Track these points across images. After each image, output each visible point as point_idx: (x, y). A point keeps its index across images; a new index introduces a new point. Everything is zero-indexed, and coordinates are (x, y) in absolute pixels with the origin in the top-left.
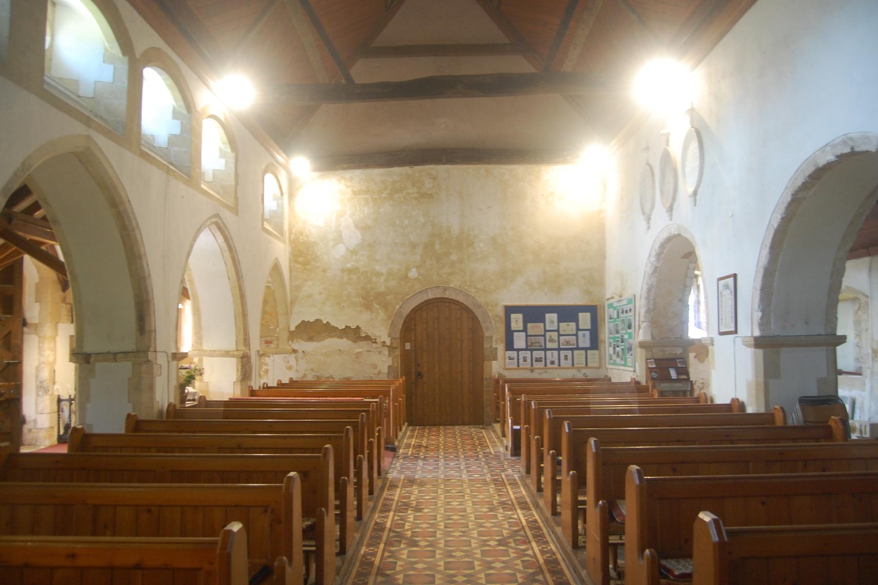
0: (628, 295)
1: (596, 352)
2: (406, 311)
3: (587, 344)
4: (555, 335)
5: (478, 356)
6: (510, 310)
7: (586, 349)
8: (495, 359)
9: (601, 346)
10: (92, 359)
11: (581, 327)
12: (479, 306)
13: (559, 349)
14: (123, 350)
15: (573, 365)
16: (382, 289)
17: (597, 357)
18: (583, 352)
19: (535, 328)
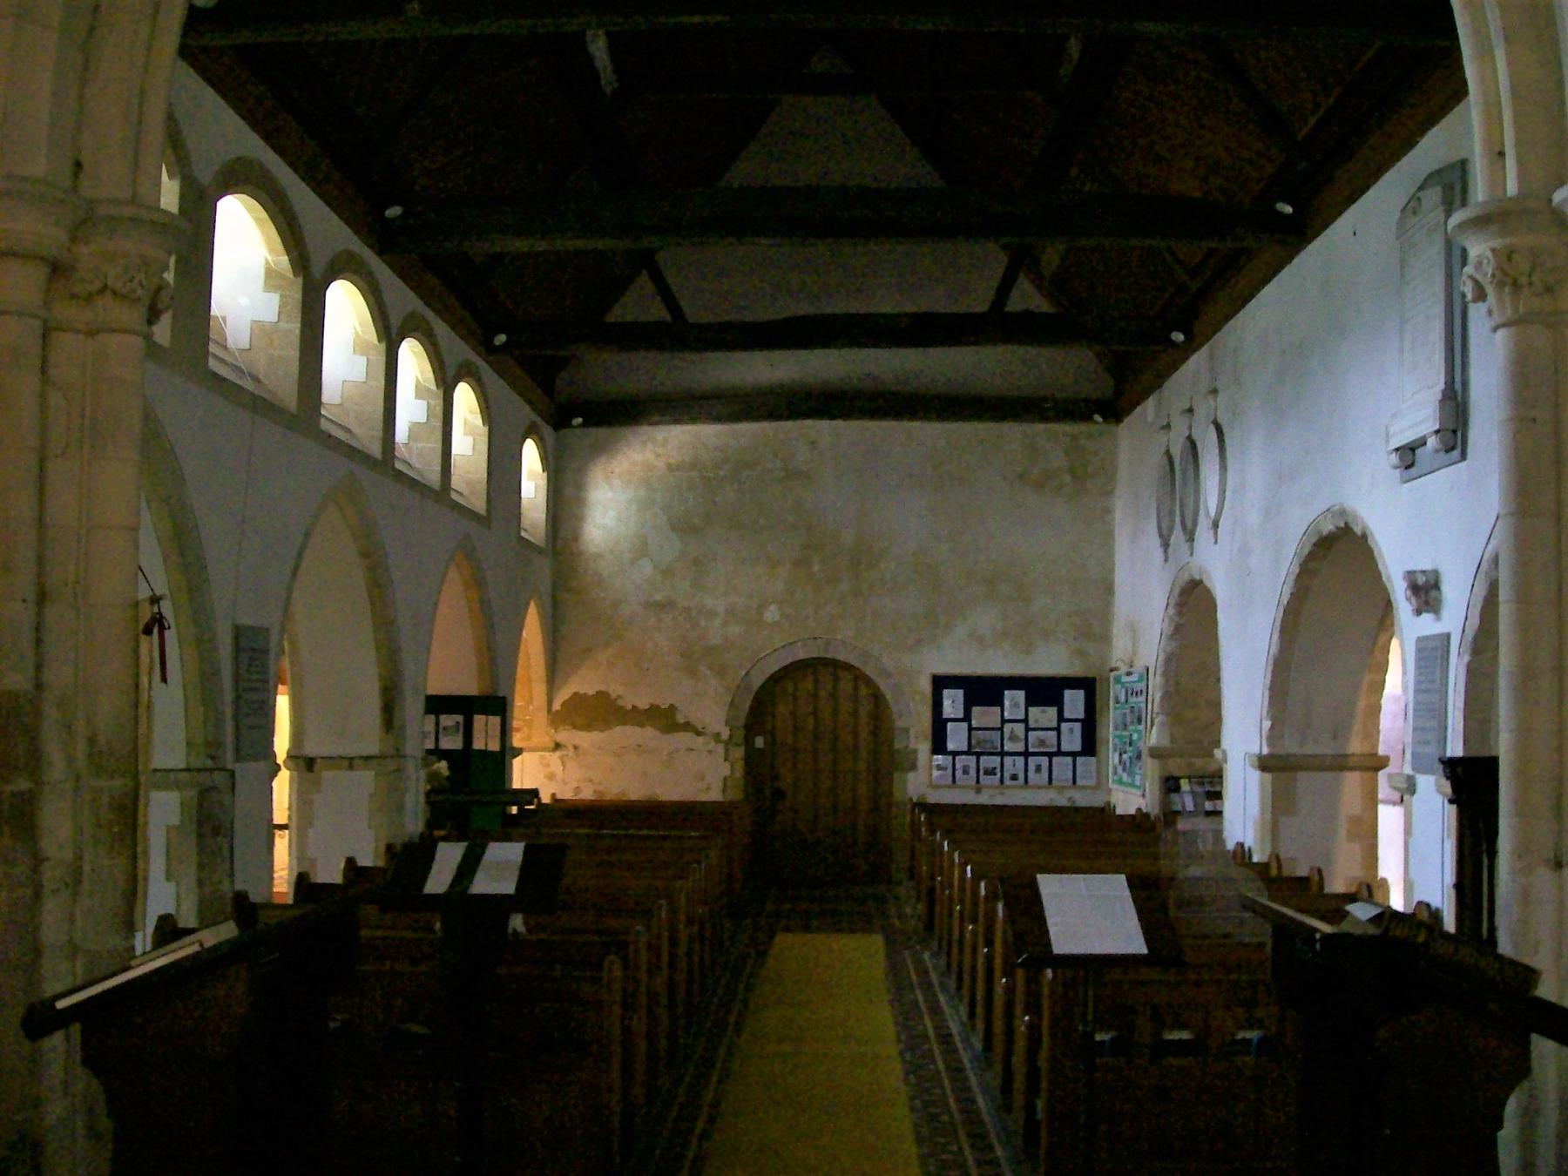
0: (1139, 666)
1: (1093, 759)
2: (758, 681)
3: (1077, 746)
4: (1019, 729)
5: (886, 760)
6: (941, 683)
7: (1074, 755)
8: (913, 767)
9: (1100, 749)
10: (316, 768)
11: (1067, 715)
12: (885, 673)
13: (1026, 754)
14: (365, 754)
15: (1074, 782)
16: (716, 641)
17: (1093, 768)
18: (1069, 759)
19: (984, 716)
